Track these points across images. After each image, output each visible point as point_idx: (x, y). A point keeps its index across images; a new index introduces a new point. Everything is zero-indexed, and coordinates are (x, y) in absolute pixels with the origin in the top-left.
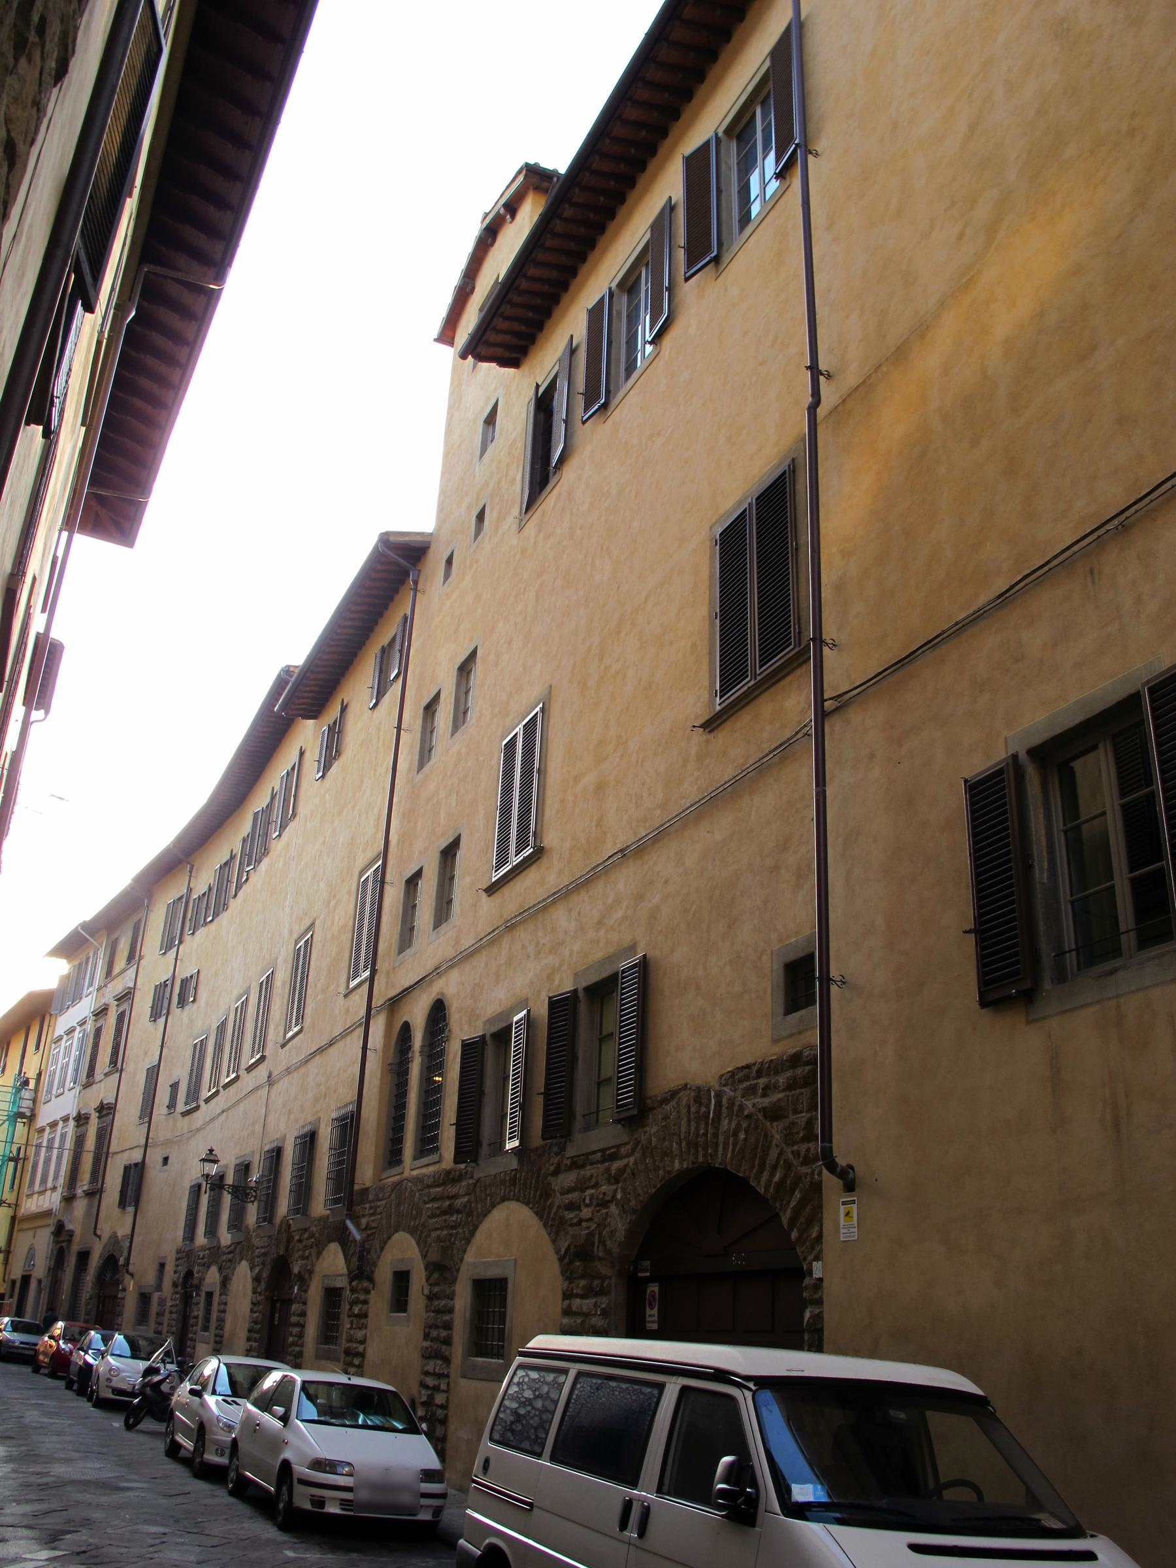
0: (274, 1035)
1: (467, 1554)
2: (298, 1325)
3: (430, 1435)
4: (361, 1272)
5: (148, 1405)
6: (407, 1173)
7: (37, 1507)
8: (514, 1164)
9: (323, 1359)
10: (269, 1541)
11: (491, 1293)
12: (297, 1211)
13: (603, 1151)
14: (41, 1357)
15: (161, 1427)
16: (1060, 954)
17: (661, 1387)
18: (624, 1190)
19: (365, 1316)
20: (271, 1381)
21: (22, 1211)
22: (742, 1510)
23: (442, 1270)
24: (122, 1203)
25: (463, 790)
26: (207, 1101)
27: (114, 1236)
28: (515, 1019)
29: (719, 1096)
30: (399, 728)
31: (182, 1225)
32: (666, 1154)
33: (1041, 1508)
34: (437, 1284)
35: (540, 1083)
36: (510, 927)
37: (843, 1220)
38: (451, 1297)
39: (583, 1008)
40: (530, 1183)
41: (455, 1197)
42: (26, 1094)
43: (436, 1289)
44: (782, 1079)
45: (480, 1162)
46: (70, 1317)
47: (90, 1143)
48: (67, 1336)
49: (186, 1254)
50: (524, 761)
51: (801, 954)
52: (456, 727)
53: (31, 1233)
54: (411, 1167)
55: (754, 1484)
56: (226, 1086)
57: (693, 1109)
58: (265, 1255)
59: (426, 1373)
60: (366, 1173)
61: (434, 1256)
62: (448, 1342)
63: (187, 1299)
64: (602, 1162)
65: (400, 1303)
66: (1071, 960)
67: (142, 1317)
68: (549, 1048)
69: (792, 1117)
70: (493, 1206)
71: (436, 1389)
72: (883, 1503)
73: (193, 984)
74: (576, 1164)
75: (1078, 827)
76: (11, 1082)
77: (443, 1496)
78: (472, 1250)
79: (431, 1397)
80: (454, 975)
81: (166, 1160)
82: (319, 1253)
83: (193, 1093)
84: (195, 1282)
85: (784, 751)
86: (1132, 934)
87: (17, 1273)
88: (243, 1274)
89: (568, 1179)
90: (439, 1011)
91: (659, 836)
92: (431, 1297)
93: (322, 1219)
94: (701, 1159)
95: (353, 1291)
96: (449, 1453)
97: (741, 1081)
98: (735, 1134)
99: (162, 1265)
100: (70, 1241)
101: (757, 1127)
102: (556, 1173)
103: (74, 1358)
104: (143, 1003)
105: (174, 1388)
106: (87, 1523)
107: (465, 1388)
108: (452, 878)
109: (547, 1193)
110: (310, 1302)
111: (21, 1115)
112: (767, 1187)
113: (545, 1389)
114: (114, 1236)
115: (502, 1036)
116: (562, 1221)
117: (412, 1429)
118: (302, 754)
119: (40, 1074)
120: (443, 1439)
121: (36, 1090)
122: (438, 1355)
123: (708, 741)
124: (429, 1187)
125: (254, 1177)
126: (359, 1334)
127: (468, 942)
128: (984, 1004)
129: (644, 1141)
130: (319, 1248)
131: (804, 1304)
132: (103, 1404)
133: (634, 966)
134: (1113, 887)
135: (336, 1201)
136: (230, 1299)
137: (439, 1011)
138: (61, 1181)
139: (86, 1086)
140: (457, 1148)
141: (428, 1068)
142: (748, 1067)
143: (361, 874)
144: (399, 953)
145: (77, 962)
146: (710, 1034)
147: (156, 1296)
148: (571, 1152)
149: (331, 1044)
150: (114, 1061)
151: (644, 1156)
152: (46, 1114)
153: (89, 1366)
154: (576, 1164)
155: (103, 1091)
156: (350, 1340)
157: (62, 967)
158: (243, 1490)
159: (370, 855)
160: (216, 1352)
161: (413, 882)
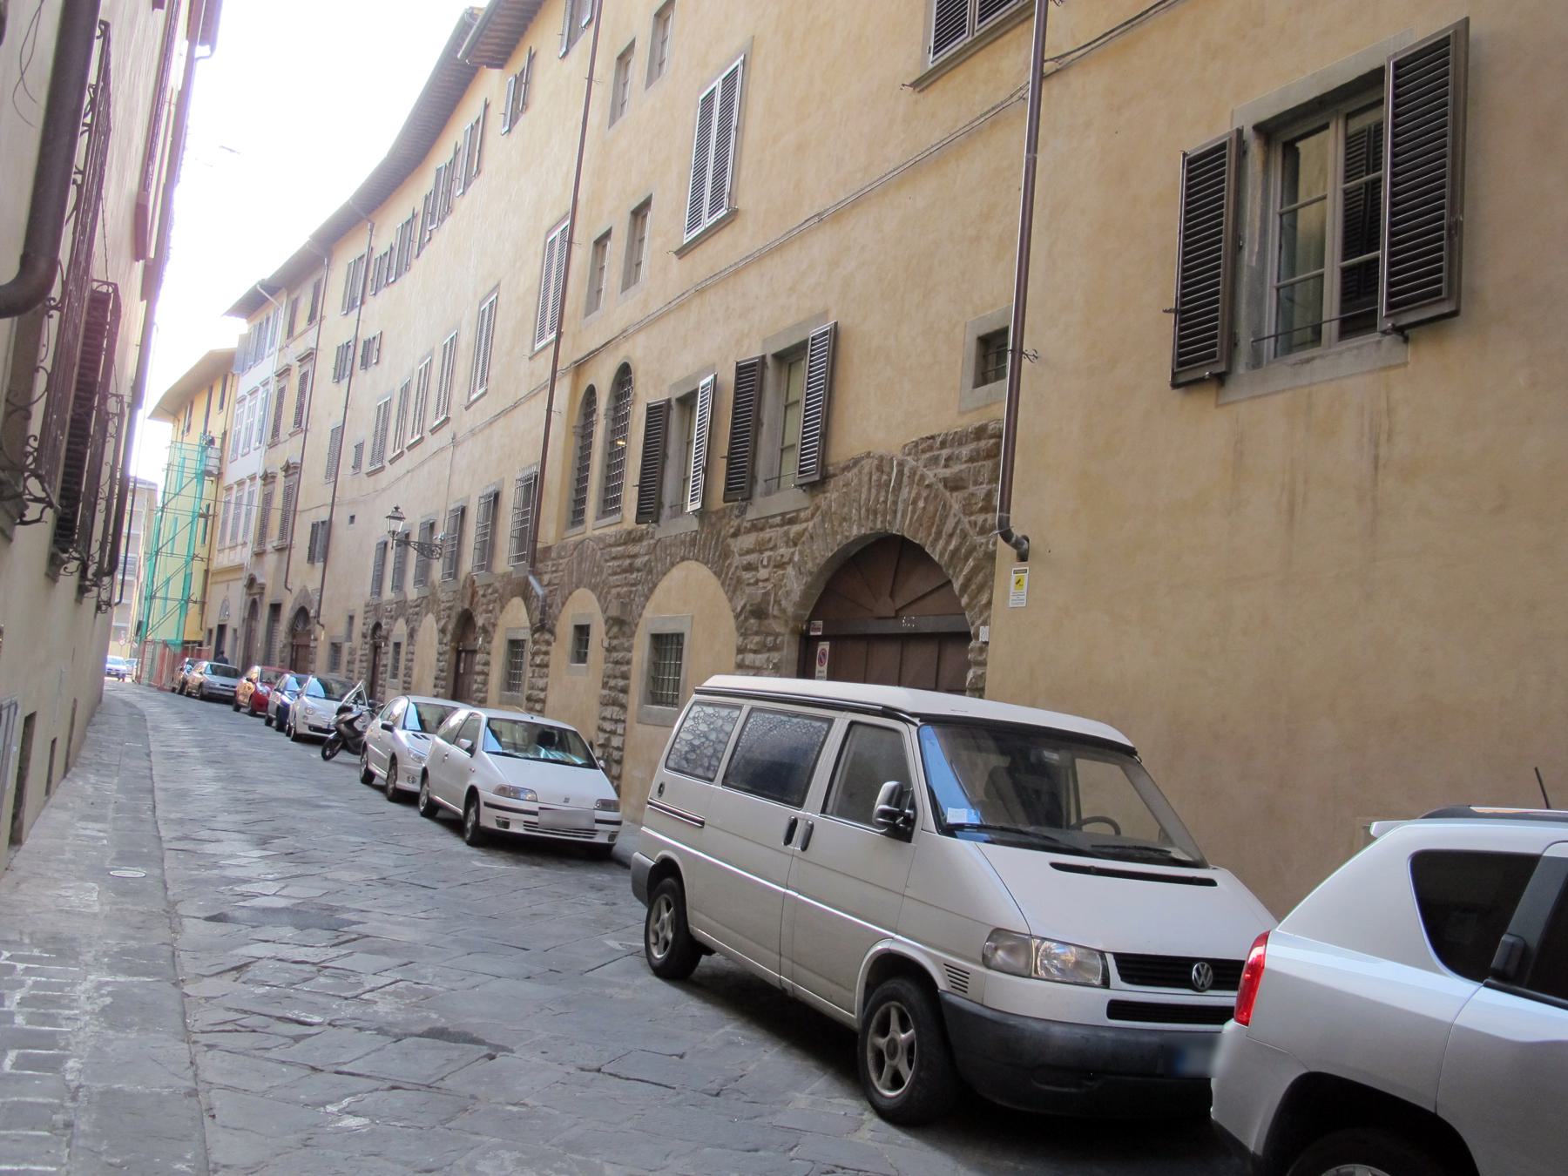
0: (458, 397)
1: (642, 865)
2: (483, 673)
3: (606, 771)
4: (543, 626)
5: (342, 740)
6: (589, 533)
7: (246, 817)
8: (694, 525)
9: (503, 703)
10: (459, 854)
11: (667, 645)
12: (481, 567)
13: (783, 515)
14: (241, 698)
15: (356, 759)
16: (1259, 340)
17: (830, 721)
18: (801, 553)
19: (547, 666)
20: (455, 720)
21: (214, 566)
22: (900, 827)
23: (621, 625)
24: (311, 559)
25: (654, 148)
26: (392, 461)
27: (304, 591)
28: (702, 383)
29: (901, 465)
30: (590, 79)
31: (369, 580)
32: (845, 519)
33: (1172, 844)
34: (615, 637)
35: (723, 447)
36: (700, 291)
37: (1013, 587)
38: (629, 650)
39: (770, 375)
40: (710, 545)
41: (635, 556)
42: (211, 452)
43: (615, 642)
44: (965, 451)
45: (662, 522)
46: (267, 661)
47: (278, 501)
48: (265, 680)
49: (374, 608)
50: (722, 114)
51: (997, 327)
52: (650, 80)
53: (224, 586)
54: (594, 526)
55: (913, 806)
56: (410, 448)
57: (874, 477)
58: (450, 608)
59: (604, 719)
60: (549, 533)
61: (614, 611)
62: (625, 690)
63: (376, 649)
64: (782, 525)
65: (580, 656)
66: (1269, 346)
67: (334, 665)
68: (734, 413)
69: (972, 489)
70: (673, 565)
71: (613, 733)
72: (1031, 829)
73: (376, 346)
74: (756, 527)
75: (1295, 211)
76: (197, 441)
77: (618, 823)
78: (650, 606)
79: (608, 740)
80: (641, 339)
81: (352, 518)
82: (502, 608)
83: (378, 455)
84: (383, 633)
85: (996, 115)
86: (1335, 324)
87: (213, 624)
88: (429, 627)
89: (748, 541)
90: (624, 374)
91: (858, 201)
92: (610, 650)
93: (507, 575)
94: (879, 525)
95: (535, 642)
96: (623, 789)
97: (923, 451)
98: (915, 502)
99: (351, 618)
100: (262, 594)
101: (936, 497)
102: (735, 535)
103: (271, 698)
104: (326, 364)
105: (365, 727)
106: (292, 831)
107: (639, 733)
108: (642, 240)
109: (726, 554)
110: (494, 652)
111: (209, 473)
112: (942, 555)
113: (720, 722)
114: (304, 591)
115: (688, 401)
116: (739, 581)
117: (591, 765)
118: (487, 106)
119: (225, 434)
120: (619, 777)
121: (222, 449)
122: (615, 702)
123: (916, 102)
124: (611, 546)
125: (440, 534)
126: (541, 683)
127: (656, 305)
128: (1175, 385)
129: (824, 505)
130: (503, 601)
131: (968, 665)
132: (299, 738)
133: (825, 333)
134: (1321, 276)
135: (519, 558)
136: (417, 649)
137: (624, 374)
138: (251, 537)
139: (272, 446)
140: (639, 509)
141: (613, 431)
142: (933, 437)
143: (549, 233)
144: (587, 315)
145: (257, 322)
146: (898, 404)
147: (346, 646)
148: (752, 514)
149: (515, 406)
150: (298, 422)
151: (823, 521)
152: (233, 473)
153: (286, 706)
154: (756, 527)
155: (289, 450)
156: (532, 688)
157: (242, 326)
158: (432, 811)
159: (557, 214)
160: (407, 690)
161: (601, 242)
